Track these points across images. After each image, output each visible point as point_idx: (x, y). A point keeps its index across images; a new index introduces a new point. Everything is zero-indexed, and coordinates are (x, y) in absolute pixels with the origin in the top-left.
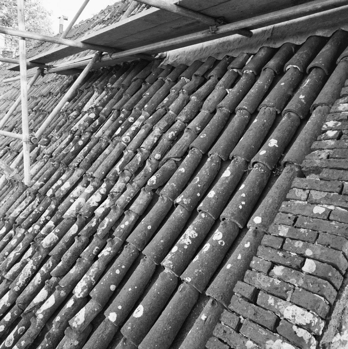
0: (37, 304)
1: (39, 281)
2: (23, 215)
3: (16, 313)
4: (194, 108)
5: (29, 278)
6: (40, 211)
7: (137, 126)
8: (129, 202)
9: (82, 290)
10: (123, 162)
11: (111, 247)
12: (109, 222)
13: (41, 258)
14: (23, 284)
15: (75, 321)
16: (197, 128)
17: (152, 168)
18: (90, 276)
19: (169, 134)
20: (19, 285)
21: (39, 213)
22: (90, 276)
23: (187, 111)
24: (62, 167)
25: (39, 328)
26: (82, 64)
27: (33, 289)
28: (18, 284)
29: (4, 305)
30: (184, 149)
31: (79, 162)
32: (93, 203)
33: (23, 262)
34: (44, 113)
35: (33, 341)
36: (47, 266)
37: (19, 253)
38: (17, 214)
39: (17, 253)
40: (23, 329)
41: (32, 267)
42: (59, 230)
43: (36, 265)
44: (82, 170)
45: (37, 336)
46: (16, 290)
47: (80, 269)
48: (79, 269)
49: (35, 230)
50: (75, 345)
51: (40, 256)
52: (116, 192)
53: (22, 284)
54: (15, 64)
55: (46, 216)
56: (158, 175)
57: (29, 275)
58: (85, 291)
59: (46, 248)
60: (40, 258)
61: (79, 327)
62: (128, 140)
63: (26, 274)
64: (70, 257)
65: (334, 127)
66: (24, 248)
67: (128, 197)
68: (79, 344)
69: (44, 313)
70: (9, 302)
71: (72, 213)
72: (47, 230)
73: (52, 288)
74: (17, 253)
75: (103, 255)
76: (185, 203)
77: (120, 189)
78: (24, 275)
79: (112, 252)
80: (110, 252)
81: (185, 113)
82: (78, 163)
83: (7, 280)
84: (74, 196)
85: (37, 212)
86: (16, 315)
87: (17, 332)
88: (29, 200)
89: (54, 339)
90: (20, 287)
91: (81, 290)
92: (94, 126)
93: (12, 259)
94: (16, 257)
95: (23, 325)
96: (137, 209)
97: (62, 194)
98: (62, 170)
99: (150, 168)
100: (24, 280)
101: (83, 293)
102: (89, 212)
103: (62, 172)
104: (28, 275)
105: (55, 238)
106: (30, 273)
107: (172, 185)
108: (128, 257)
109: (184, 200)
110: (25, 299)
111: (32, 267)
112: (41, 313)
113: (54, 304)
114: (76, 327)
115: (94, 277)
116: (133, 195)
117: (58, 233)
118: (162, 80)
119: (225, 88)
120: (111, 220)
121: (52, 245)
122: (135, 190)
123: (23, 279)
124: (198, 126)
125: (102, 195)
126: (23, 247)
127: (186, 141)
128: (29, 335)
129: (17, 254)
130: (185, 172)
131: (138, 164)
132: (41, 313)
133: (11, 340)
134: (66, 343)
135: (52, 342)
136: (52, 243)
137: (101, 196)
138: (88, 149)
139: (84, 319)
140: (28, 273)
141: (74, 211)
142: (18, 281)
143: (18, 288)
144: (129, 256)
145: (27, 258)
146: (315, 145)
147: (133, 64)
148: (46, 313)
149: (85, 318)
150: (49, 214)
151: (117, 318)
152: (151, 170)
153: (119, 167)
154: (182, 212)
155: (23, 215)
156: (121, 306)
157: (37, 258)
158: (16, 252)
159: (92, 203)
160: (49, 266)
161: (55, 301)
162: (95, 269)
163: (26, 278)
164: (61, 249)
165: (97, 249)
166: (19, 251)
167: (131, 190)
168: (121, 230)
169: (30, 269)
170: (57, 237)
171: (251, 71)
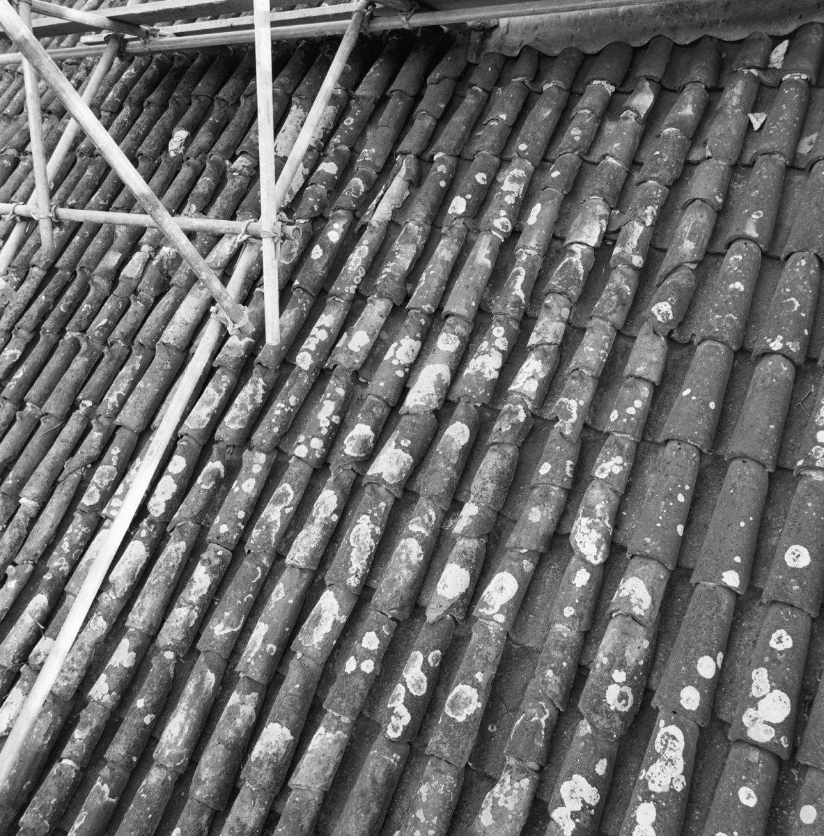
0: (456, 600)
1: (419, 555)
2: (237, 421)
3: (388, 631)
4: (680, 153)
5: (371, 554)
6: (292, 407)
7: (517, 195)
8: (605, 360)
9: (599, 548)
10: (525, 277)
11: (621, 455)
12: (579, 407)
13: (386, 508)
14: (364, 570)
15: (636, 605)
16: (717, 197)
17: (630, 285)
18: (600, 518)
19: (646, 211)
20: (356, 573)
21: (289, 411)
22: (600, 518)
23: (668, 162)
24: (301, 297)
25: (499, 642)
26: (291, 33)
27: (411, 574)
29: (335, 621)
30: (705, 243)
31: (357, 283)
32: (490, 372)
34: (96, 162)
35: (496, 670)
36: (427, 521)
37: (292, 508)
38: (204, 421)
39: (285, 507)
40: (437, 655)
41: (372, 529)
42: (409, 442)
43: (379, 524)
44: (385, 300)
45: (499, 658)
46: (354, 585)
47: (551, 510)
48: (548, 510)
49: (315, 449)
50: (646, 647)
51: (383, 504)
52: (550, 344)
53: (361, 569)
54: (53, 18)
55: (331, 416)
56: (672, 301)
57: (371, 547)
58: (603, 548)
59: (394, 484)
60: (383, 509)
61: (648, 613)
62: (507, 226)
63: (365, 547)
64: (494, 491)
66: (299, 494)
67: (602, 352)
68: (650, 646)
69: (506, 611)
70: (344, 613)
71: (430, 400)
72: (360, 446)
73: (473, 561)
74: (285, 507)
75: (611, 472)
76: (793, 350)
77: (557, 336)
78: (360, 549)
79: (625, 464)
80: (622, 465)
81: (665, 165)
82: (356, 287)
83: (301, 569)
84: (402, 363)
85: (286, 410)
86: (388, 634)
87: (429, 665)
88: (225, 385)
89: (574, 651)
90: (360, 576)
91: (595, 549)
92: (355, 194)
93: (279, 524)
94: (286, 519)
95: (436, 648)
96: (652, 372)
97: (357, 361)
98: (304, 305)
99: (627, 287)
100: (365, 561)
101: (601, 553)
103: (305, 309)
104: (369, 549)
105: (406, 460)
106: (373, 544)
107: (727, 318)
108: (689, 469)
109: (790, 344)
110: (401, 598)
111: (373, 529)
112: (498, 613)
113: (518, 590)
114: (643, 614)
115: (608, 519)
116: (609, 345)
117: (409, 448)
118: (523, 82)
119: (745, 113)
120: (582, 403)
121: (404, 475)
122: (609, 335)
123: (362, 559)
124: (718, 194)
125: (503, 352)
126: (296, 494)
128: (487, 660)
129: (288, 510)
130: (745, 290)
131: (581, 278)
132: (498, 613)
133: (422, 681)
135: (572, 657)
136: (403, 471)
137: (500, 354)
138: (370, 250)
139: (650, 598)
140: (368, 545)
141: (432, 394)
142: (351, 565)
143: (357, 580)
144: (691, 465)
145: (331, 515)
148: (508, 610)
149: (652, 596)
150: (336, 409)
151: (740, 579)
152: (629, 290)
153: (522, 288)
154: (786, 369)
156: (739, 556)
158: (283, 506)
159: (486, 371)
160: (430, 519)
161: (519, 583)
162: (603, 502)
163: (367, 557)
164: (448, 479)
166: (288, 503)
167: (601, 336)
168: (632, 419)
169: (370, 535)
170: (411, 457)
171: (804, 77)
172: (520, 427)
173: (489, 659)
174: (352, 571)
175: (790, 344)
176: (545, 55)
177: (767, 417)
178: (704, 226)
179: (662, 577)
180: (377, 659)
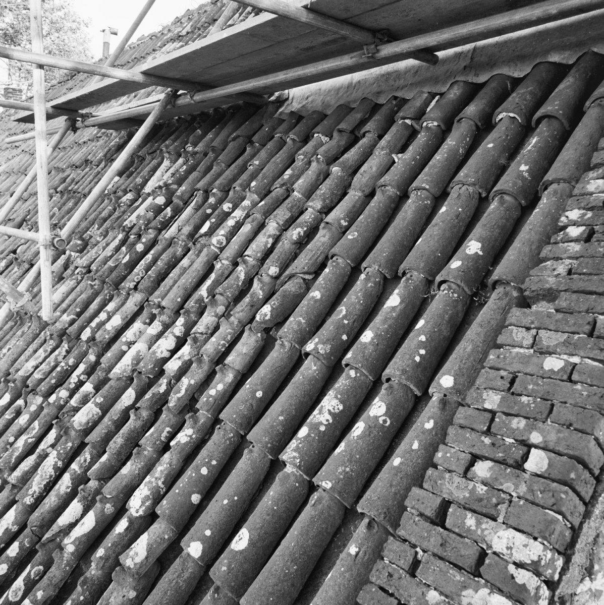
0: (64, 527)
1: (68, 487)
2: (41, 373)
3: (28, 543)
4: (337, 187)
5: (50, 481)
6: (69, 366)
7: (238, 219)
8: (223, 350)
9: (143, 503)
10: (213, 281)
11: (193, 428)
12: (190, 385)
13: (71, 448)
14: (39, 493)
15: (131, 557)
16: (342, 222)
17: (263, 291)
18: (156, 479)
19: (294, 232)
20: (33, 494)
21: (67, 369)
23: (324, 193)
25: (68, 568)
27: (57, 501)
29: (7, 528)
30: (320, 258)
32: (162, 352)
33: (40, 454)
34: (76, 197)
35: (57, 591)
36: (82, 461)
37: (34, 439)
38: (29, 371)
39: (29, 438)
40: (40, 570)
41: (55, 462)
42: (102, 399)
43: (62, 459)
45: (63, 582)
46: (28, 503)
47: (140, 466)
48: (136, 466)
49: (61, 398)
50: (131, 598)
51: (70, 444)
52: (202, 333)
53: (37, 492)
55: (80, 375)
56: (274, 304)
57: (51, 476)
58: (147, 504)
59: (80, 430)
60: (69, 448)
61: (138, 566)
62: (222, 243)
63: (46, 475)
64: (121, 445)
66: (42, 430)
67: (222, 342)
68: (137, 597)
69: (77, 543)
70: (16, 524)
72: (81, 399)
73: (90, 498)
74: (29, 438)
75: (179, 441)
76: (321, 352)
77: (208, 328)
80: (190, 436)
81: (320, 196)
82: (135, 283)
83: (13, 485)
85: (65, 368)
86: (28, 546)
87: (30, 576)
89: (94, 587)
90: (35, 497)
91: (140, 503)
92: (162, 218)
93: (20, 450)
94: (27, 446)
97: (107, 337)
98: (108, 295)
99: (261, 292)
100: (42, 486)
101: (144, 508)
103: (108, 297)
104: (48, 477)
105: (95, 413)
106: (53, 473)
107: (298, 321)
109: (320, 346)
111: (56, 462)
112: (71, 543)
113: (94, 527)
114: (132, 567)
115: (163, 480)
116: (231, 338)
117: (100, 404)
119: (391, 152)
120: (192, 382)
121: (90, 424)
122: (234, 329)
123: (41, 484)
124: (344, 219)
125: (177, 337)
126: (40, 429)
128: (51, 581)
129: (30, 441)
130: (321, 297)
131: (240, 284)
132: (71, 543)
133: (20, 590)
135: (90, 593)
136: (91, 421)
137: (175, 339)
138: (153, 258)
139: (146, 553)
140: (49, 474)
141: (128, 366)
142: (31, 488)
143: (32, 499)
144: (224, 443)
145: (48, 448)
148: (79, 543)
149: (148, 552)
150: (85, 370)
151: (203, 551)
152: (262, 294)
153: (207, 290)
154: (315, 368)
155: (41, 373)
156: (211, 530)
157: (64, 448)
158: (28, 436)
159: (159, 351)
160: (85, 461)
161: (96, 522)
162: (165, 466)
163: (45, 483)
164: (106, 431)
166: (32, 435)
167: (227, 329)
168: (211, 399)
169: (52, 467)
170: (100, 411)
171: (436, 124)
172: (159, 396)
173: (53, 582)
174: (30, 492)
175: (320, 346)
176: (347, 114)
177: (281, 409)
178: (323, 244)
179: (166, 537)
180: (12, 565)
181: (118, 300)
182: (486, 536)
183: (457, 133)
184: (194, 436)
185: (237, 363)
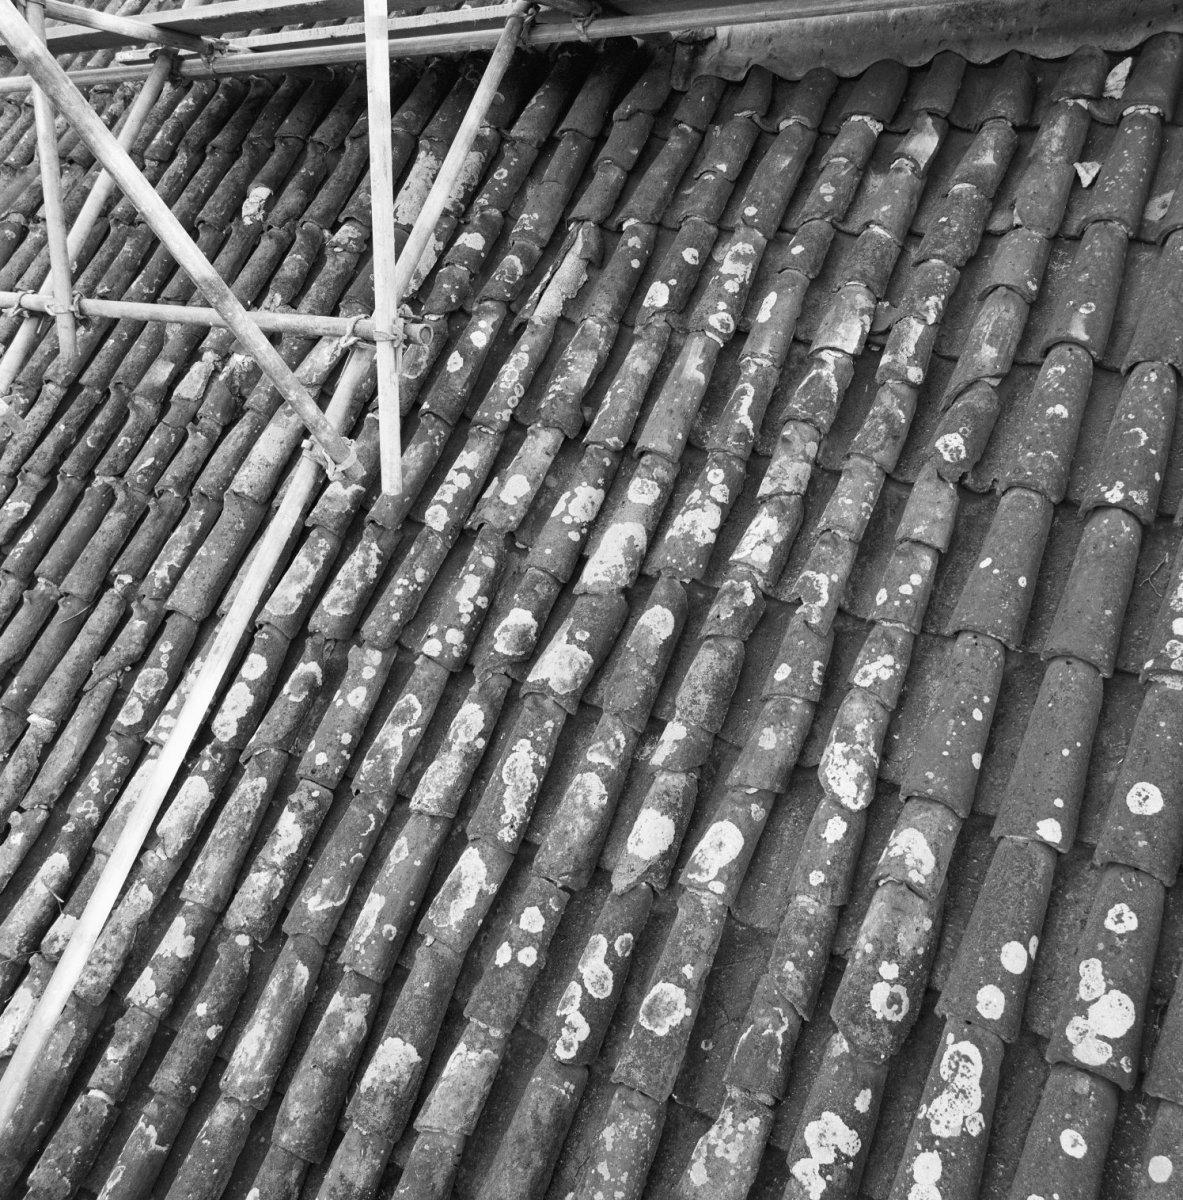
0: (655, 861)
1: (602, 797)
2: (340, 604)
3: (556, 905)
4: (976, 219)
5: (533, 795)
6: (419, 584)
7: (742, 279)
8: (868, 517)
9: (859, 787)
10: (754, 398)
11: (891, 653)
12: (832, 584)
13: (554, 729)
14: (522, 819)
15: (913, 868)
16: (1029, 283)
17: (904, 410)
18: (862, 744)
19: (928, 303)
20: (512, 822)
21: (415, 590)
23: (959, 232)
24: (431, 427)
25: (716, 921)
27: (591, 824)
28: (505, 819)
29: (481, 892)
30: (1012, 349)
32: (704, 534)
33: (466, 754)
34: (137, 233)
35: (712, 961)
37: (419, 729)
38: (293, 605)
39: (410, 728)
40: (627, 940)
41: (534, 759)
42: (587, 634)
43: (544, 752)
45: (717, 944)
46: (508, 839)
47: (791, 732)
48: (786, 733)
49: (453, 645)
50: (927, 929)
51: (549, 724)
52: (790, 494)
53: (518, 817)
55: (476, 597)
56: (965, 431)
57: (533, 786)
58: (865, 787)
59: (566, 695)
60: (550, 730)
61: (930, 879)
62: (729, 325)
63: (524, 786)
64: (709, 705)
65: (639, 41)
66: (429, 710)
67: (865, 505)
68: (934, 927)
69: (726, 877)
70: (493, 881)
72: (517, 640)
73: (680, 806)
74: (410, 728)
75: (878, 678)
76: (1138, 502)
77: (800, 482)
80: (893, 667)
81: (954, 237)
82: (510, 412)
83: (432, 817)
85: (411, 588)
86: (557, 909)
87: (615, 955)
88: (323, 552)
89: (824, 934)
90: (516, 827)
91: (855, 789)
92: (509, 278)
93: (400, 752)
94: (411, 744)
95: (625, 930)
97: (512, 518)
98: (437, 437)
99: (901, 413)
100: (523, 806)
101: (863, 794)
102: (697, 563)
103: (437, 443)
104: (529, 788)
105: (583, 661)
106: (535, 781)
109: (1134, 494)
110: (576, 859)
111: (536, 760)
112: (715, 880)
113: (744, 847)
114: (923, 881)
115: (872, 744)
116: (875, 495)
117: (587, 643)
119: (1070, 162)
120: (835, 578)
121: (580, 682)
122: (874, 481)
123: (520, 802)
124: (1031, 279)
125: (722, 505)
126: (424, 708)
127: (1010, 324)
128: (699, 947)
129: (413, 733)
130: (1070, 416)
131: (835, 400)
132: (715, 880)
133: (606, 978)
134: (903, 929)
135: (821, 943)
136: (579, 676)
137: (718, 509)
138: (531, 359)
139: (933, 858)
140: (528, 782)
141: (621, 566)
142: (504, 812)
143: (512, 832)
144: (991, 667)
145: (476, 739)
146: (998, 223)
147: (567, 54)
148: (729, 876)
149: (936, 856)
150: (482, 587)
151: (1063, 831)
152: (903, 416)
153: (750, 414)
154: (1128, 529)
155: (340, 604)
156: (1062, 798)
157: (541, 732)
158: (406, 726)
159: (698, 533)
160: (618, 746)
161: (745, 837)
162: (866, 721)
163: (526, 800)
164: (644, 688)
165: (819, 669)
166: (414, 722)
167: (863, 482)
168: (908, 601)
169: (531, 768)
170: (589, 657)
171: (1155, 110)
179: (950, 828)
181: (482, 446)
182: (175, 1099)
183: (420, 448)
184: (898, 667)
185: (936, 534)
